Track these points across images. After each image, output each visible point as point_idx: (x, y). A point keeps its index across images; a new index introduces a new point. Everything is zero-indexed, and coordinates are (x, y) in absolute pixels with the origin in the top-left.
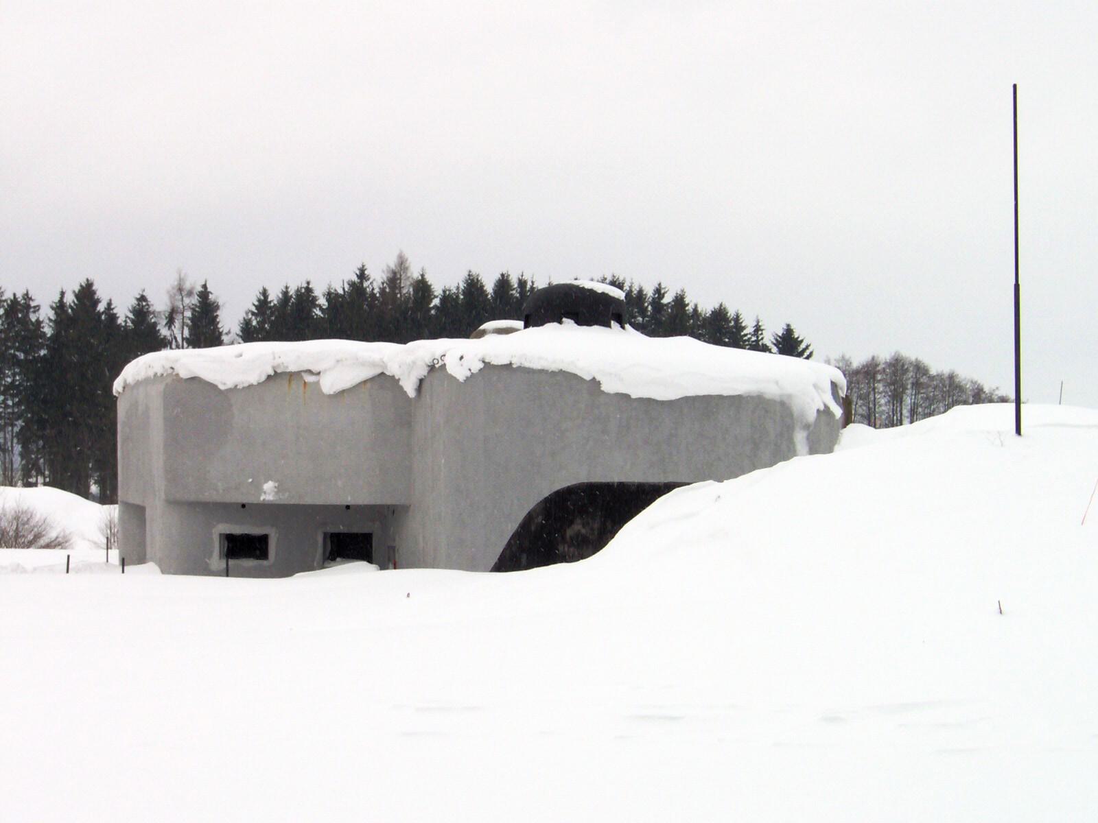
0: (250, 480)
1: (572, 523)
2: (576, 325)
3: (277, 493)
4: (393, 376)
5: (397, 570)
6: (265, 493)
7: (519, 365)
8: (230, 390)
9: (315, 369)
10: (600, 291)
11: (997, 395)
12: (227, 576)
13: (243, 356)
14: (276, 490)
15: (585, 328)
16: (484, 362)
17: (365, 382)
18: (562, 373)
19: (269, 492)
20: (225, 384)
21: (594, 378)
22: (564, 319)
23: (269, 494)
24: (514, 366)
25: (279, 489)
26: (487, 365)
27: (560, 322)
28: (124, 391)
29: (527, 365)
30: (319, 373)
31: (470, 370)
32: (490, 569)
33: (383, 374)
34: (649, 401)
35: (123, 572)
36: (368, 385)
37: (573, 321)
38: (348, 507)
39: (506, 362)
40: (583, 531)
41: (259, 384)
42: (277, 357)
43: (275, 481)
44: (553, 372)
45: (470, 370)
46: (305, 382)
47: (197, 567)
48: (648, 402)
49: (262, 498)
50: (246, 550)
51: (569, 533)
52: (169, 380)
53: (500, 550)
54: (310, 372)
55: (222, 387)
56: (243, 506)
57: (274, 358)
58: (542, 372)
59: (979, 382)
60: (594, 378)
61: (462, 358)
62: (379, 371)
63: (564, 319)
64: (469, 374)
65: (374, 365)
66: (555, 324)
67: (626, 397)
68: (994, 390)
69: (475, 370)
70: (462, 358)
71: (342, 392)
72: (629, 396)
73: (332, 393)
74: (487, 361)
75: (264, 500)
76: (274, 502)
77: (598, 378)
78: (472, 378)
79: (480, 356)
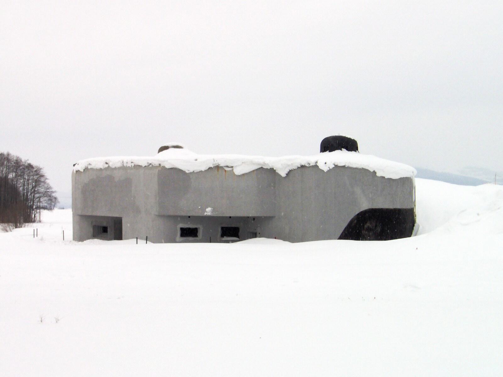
0: (200, 207)
1: (366, 223)
2: (347, 151)
3: (212, 212)
4: (374, 172)
5: (211, 243)
6: (207, 212)
7: (348, 166)
8: (191, 173)
9: (230, 165)
10: (353, 139)
11: (27, 163)
12: (210, 242)
13: (198, 160)
14: (212, 211)
15: (350, 152)
16: (335, 165)
17: (253, 171)
18: (363, 169)
19: (209, 211)
20: (189, 171)
21: (374, 171)
22: (342, 149)
23: (209, 212)
24: (346, 166)
25: (213, 211)
26: (336, 166)
27: (341, 150)
28: (84, 171)
29: (351, 166)
30: (232, 167)
31: (329, 168)
32: (338, 238)
33: (262, 167)
34: (390, 179)
35: (146, 243)
36: (255, 172)
37: (345, 150)
38: (230, 217)
39: (343, 165)
40: (370, 226)
41: (205, 171)
42: (215, 161)
43: (212, 208)
44: (360, 169)
45: (329, 168)
46: (225, 170)
47: (172, 240)
48: (390, 179)
49: (205, 214)
50: (189, 234)
51: (366, 226)
52: (160, 169)
53: (341, 232)
54: (227, 167)
55: (187, 172)
56: (189, 217)
57: (214, 161)
58: (356, 168)
59: (20, 157)
60: (374, 171)
61: (326, 163)
62: (260, 167)
63: (342, 149)
64: (329, 169)
65: (259, 164)
66: (340, 151)
67: (383, 177)
68: (26, 161)
69: (331, 168)
70: (326, 163)
71: (243, 175)
72: (385, 177)
73: (240, 175)
74: (336, 164)
75: (206, 215)
76: (211, 216)
77: (376, 171)
78: (330, 171)
79: (333, 163)
